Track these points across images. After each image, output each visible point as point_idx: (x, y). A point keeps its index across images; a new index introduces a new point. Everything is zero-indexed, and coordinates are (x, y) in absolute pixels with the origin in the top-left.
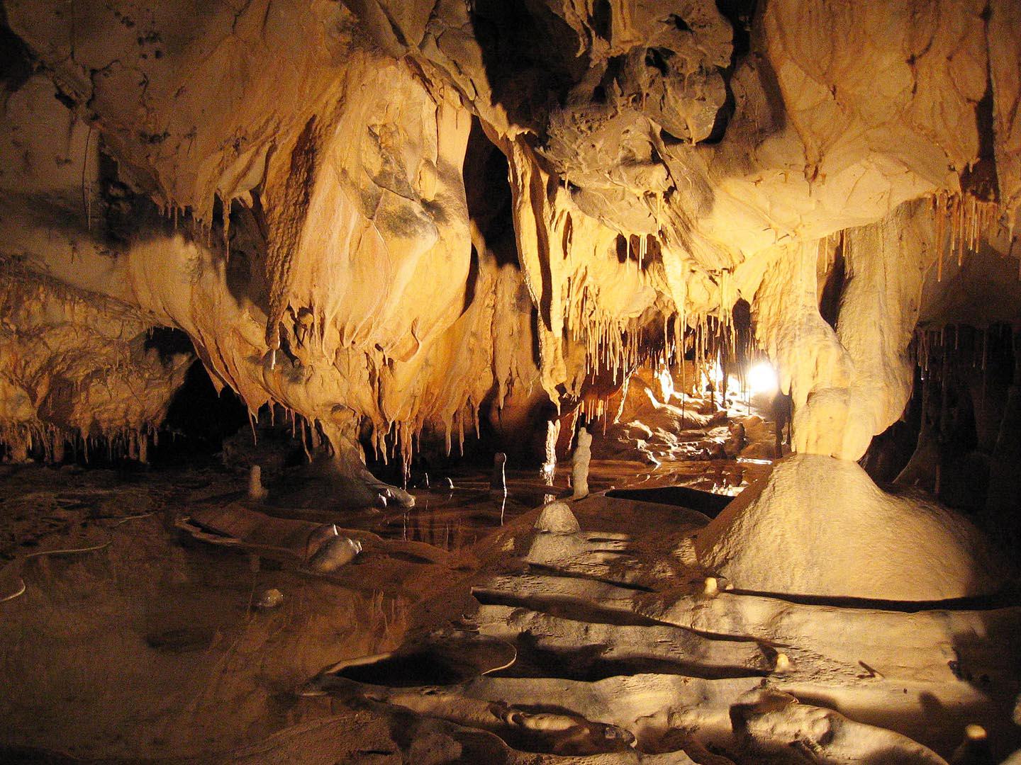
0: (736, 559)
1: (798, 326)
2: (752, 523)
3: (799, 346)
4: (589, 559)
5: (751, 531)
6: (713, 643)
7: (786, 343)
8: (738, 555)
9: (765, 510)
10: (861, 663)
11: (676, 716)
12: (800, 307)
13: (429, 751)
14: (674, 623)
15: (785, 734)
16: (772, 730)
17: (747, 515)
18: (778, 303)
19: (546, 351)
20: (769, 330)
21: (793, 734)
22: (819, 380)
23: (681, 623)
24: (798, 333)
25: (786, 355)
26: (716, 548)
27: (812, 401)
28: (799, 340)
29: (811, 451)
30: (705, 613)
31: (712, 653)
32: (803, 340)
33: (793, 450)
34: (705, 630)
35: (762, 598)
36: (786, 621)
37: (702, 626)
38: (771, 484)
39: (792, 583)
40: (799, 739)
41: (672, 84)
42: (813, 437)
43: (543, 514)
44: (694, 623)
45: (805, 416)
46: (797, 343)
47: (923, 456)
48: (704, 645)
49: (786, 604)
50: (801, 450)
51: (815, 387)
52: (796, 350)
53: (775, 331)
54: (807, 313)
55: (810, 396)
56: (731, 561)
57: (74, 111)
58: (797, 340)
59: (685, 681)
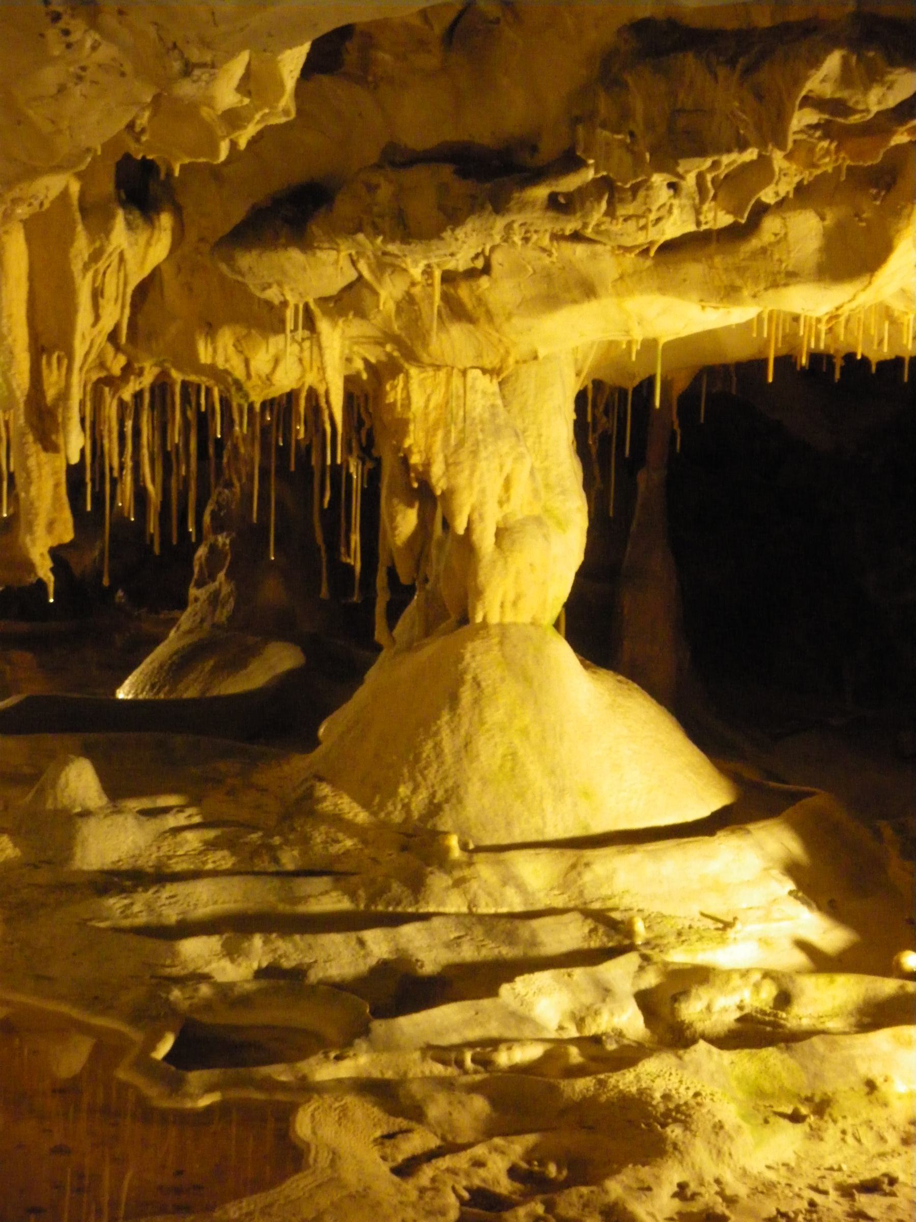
0: (454, 801)
1: (479, 427)
2: (460, 741)
3: (486, 458)
4: (180, 845)
5: (463, 754)
6: (536, 923)
7: (464, 455)
8: (454, 795)
9: (476, 718)
10: (703, 914)
11: (588, 1020)
12: (479, 395)
13: (450, 1114)
14: (441, 910)
15: (725, 1010)
16: (709, 1008)
17: (445, 733)
18: (443, 390)
19: (40, 489)
20: (430, 433)
21: (734, 1007)
22: (507, 508)
23: (450, 909)
24: (480, 437)
25: (467, 472)
26: (403, 791)
27: (506, 543)
28: (486, 447)
29: (509, 618)
30: (479, 887)
31: (543, 937)
32: (491, 448)
33: (479, 619)
34: (492, 911)
35: (531, 852)
36: (587, 877)
37: (487, 905)
38: (468, 677)
39: (545, 823)
40: (746, 1011)
41: (682, 207)
42: (511, 597)
43: (62, 780)
44: (472, 904)
45: (500, 564)
46: (483, 454)
47: (650, 607)
48: (524, 929)
49: (570, 855)
50: (494, 618)
51: (505, 518)
52: (483, 465)
53: (440, 434)
54: (489, 403)
55: (497, 535)
56: (446, 807)
57: (425, 358)
58: (482, 448)
59: (569, 975)
